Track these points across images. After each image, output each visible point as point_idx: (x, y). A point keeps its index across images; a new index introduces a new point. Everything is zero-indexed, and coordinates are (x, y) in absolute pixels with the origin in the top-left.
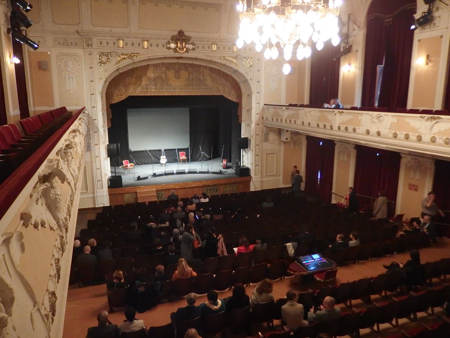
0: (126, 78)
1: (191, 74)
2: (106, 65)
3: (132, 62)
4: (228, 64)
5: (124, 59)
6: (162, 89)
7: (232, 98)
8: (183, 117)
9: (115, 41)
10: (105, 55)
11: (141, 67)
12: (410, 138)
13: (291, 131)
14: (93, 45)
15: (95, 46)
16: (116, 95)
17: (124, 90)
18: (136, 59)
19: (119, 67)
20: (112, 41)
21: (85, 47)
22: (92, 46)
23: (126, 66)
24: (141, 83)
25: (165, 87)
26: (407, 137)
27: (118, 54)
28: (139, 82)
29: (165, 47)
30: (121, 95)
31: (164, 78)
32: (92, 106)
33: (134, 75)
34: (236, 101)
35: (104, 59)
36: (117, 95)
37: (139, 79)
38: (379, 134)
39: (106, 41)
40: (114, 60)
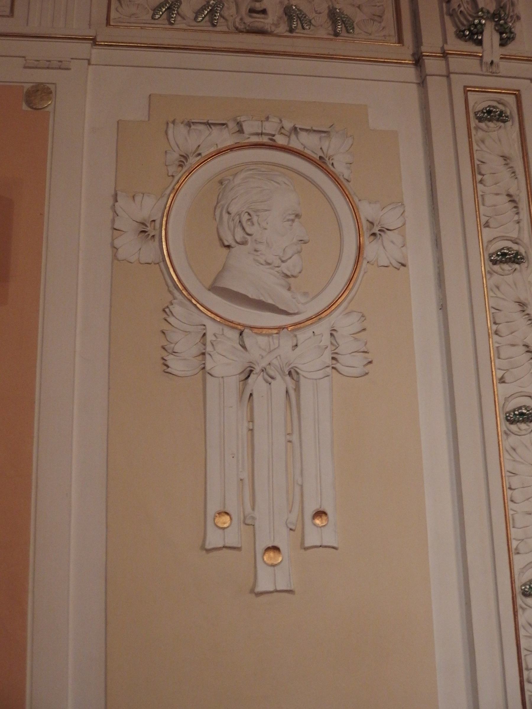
14: (518, 28)
21: (431, 42)
22: (506, 37)
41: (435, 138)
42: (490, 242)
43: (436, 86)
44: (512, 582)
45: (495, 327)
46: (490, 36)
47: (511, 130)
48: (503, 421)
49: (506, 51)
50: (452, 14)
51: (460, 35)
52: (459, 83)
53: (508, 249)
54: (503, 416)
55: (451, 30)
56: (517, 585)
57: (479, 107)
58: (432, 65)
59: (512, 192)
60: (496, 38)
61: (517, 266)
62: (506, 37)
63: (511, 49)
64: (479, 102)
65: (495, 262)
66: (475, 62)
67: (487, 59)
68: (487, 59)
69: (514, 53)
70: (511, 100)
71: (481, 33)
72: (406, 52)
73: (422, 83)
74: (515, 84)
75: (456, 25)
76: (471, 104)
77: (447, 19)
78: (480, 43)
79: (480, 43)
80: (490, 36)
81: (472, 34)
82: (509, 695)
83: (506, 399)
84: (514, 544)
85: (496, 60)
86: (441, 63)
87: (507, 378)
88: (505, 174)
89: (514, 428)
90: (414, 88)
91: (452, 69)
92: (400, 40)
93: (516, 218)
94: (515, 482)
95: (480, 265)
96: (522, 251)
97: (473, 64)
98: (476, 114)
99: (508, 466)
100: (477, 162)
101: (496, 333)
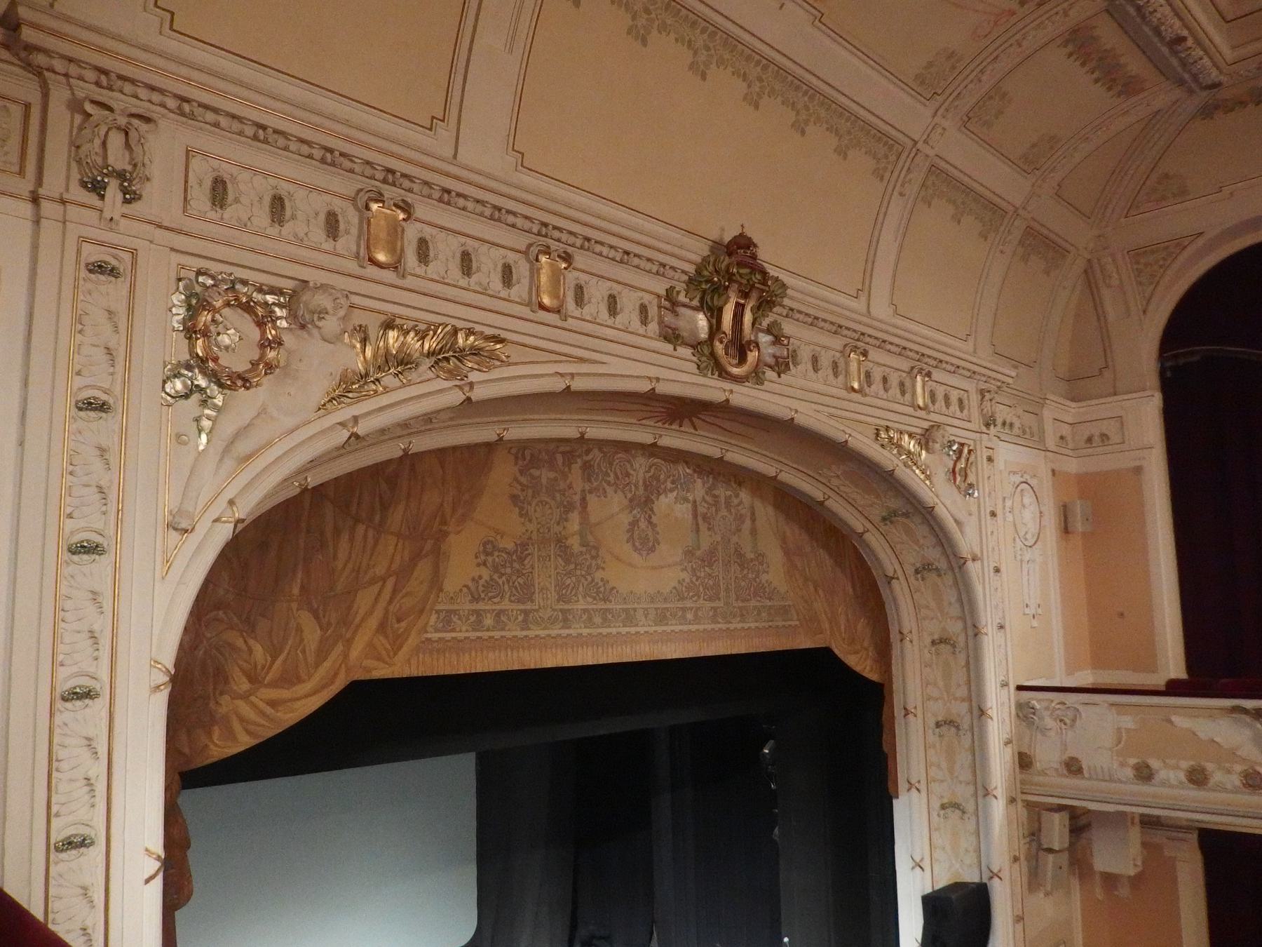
0: (337, 531)
1: (703, 527)
2: (246, 402)
3: (456, 397)
4: (903, 473)
5: (404, 362)
6: (566, 623)
7: (861, 663)
8: (446, 784)
9: (338, 205)
10: (248, 308)
11: (441, 453)
12: (1212, 782)
13: (1142, 815)
14: (148, 190)
15: (160, 195)
16: (244, 685)
17: (312, 635)
18: (488, 384)
19: (361, 429)
20: (321, 203)
21: (53, 184)
22: (130, 197)
23: (405, 426)
24: (436, 583)
25: (581, 605)
26: (1197, 777)
27: (359, 318)
28: (423, 570)
29: (653, 327)
30: (289, 678)
31: (575, 543)
32: (60, 831)
33: (397, 517)
34: (874, 677)
35: (234, 338)
36: (253, 679)
37: (428, 542)
38: (1073, 767)
39: (266, 187)
40: (321, 359)
41: (39, 283)
42: (80, 389)
43: (50, 229)
44: (48, 838)
45: (71, 468)
46: (113, 191)
47: (122, 286)
48: (66, 552)
49: (127, 209)
50: (79, 162)
51: (83, 184)
52: (74, 231)
53: (95, 398)
54: (65, 548)
55: (75, 176)
56: (52, 841)
57: (92, 260)
58: (47, 207)
59: (110, 345)
60: (120, 196)
61: (104, 415)
62: (130, 197)
63: (136, 207)
64: (93, 254)
65: (80, 409)
66: (96, 214)
67: (107, 215)
68: (107, 215)
69: (136, 213)
70: (127, 257)
71: (105, 189)
72: (26, 186)
73: (37, 222)
74: (136, 243)
75: (80, 173)
76: (84, 255)
77: (74, 165)
78: (102, 197)
79: (102, 197)
80: (113, 191)
81: (97, 188)
82: (58, 260)
83: (72, 533)
84: (54, 809)
85: (115, 217)
86: (60, 208)
87: (75, 515)
88: (107, 328)
89: (76, 558)
90: (29, 224)
91: (69, 207)
92: (21, 172)
93: (111, 370)
94: (68, 604)
95: (64, 406)
96: (111, 401)
97: (91, 216)
98: (87, 265)
99: (64, 590)
100: (80, 312)
101: (71, 473)
